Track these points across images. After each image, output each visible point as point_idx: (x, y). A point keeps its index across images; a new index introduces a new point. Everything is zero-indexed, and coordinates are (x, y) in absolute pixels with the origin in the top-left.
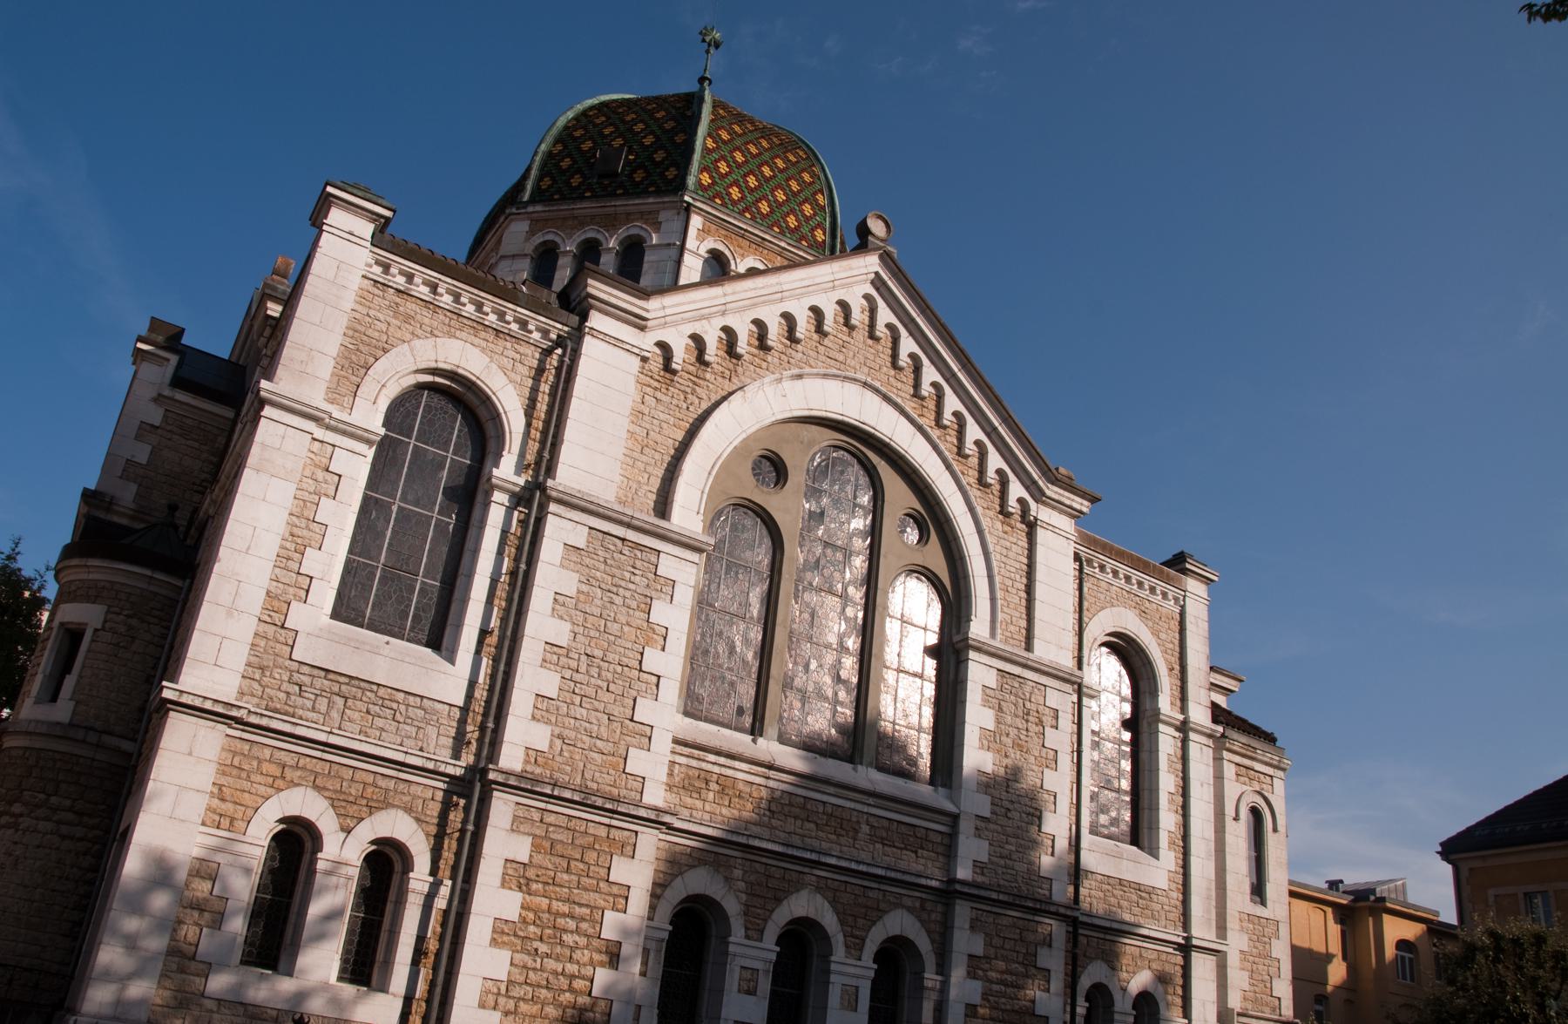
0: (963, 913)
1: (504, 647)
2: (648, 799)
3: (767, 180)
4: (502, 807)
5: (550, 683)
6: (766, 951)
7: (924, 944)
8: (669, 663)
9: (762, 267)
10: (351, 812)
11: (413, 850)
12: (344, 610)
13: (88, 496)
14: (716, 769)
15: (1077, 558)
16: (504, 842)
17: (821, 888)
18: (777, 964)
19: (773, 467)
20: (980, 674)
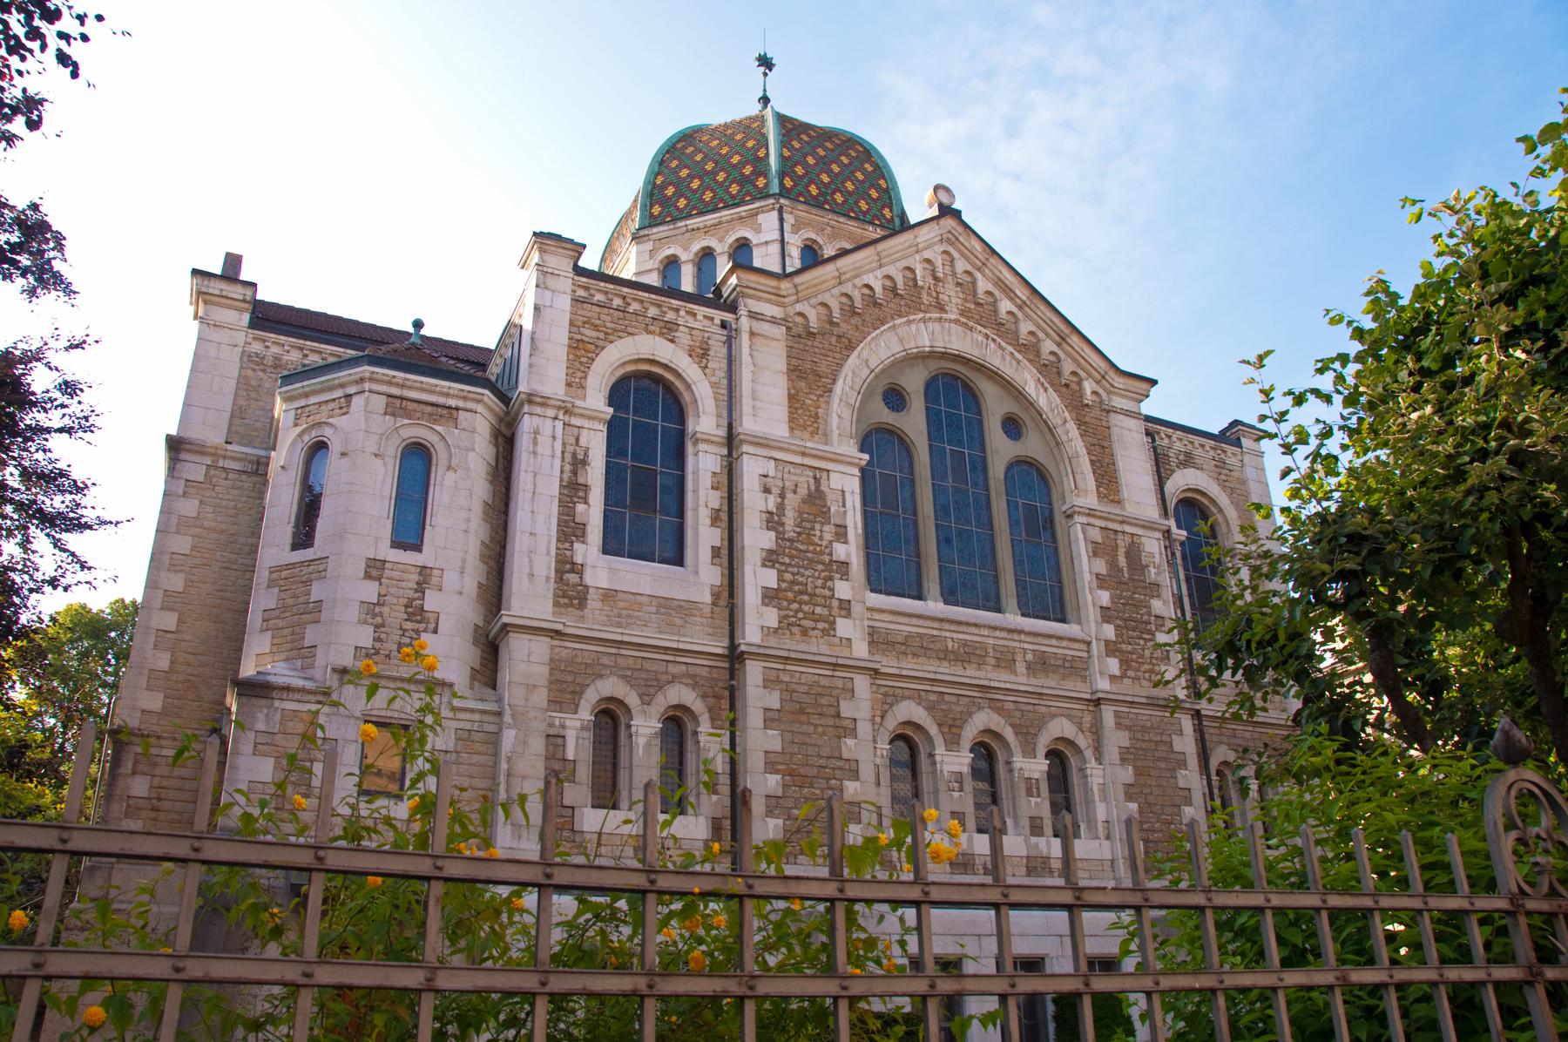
0: (1108, 713)
1: (729, 556)
2: (856, 654)
3: (837, 175)
4: (754, 672)
5: (770, 578)
6: (1038, 767)
7: (1082, 741)
8: (851, 551)
9: (848, 246)
10: (649, 688)
11: (619, 695)
12: (611, 546)
13: (175, 446)
14: (991, 641)
15: (1148, 433)
16: (758, 696)
17: (918, 696)
18: (1049, 773)
19: (895, 398)
20: (445, 412)
